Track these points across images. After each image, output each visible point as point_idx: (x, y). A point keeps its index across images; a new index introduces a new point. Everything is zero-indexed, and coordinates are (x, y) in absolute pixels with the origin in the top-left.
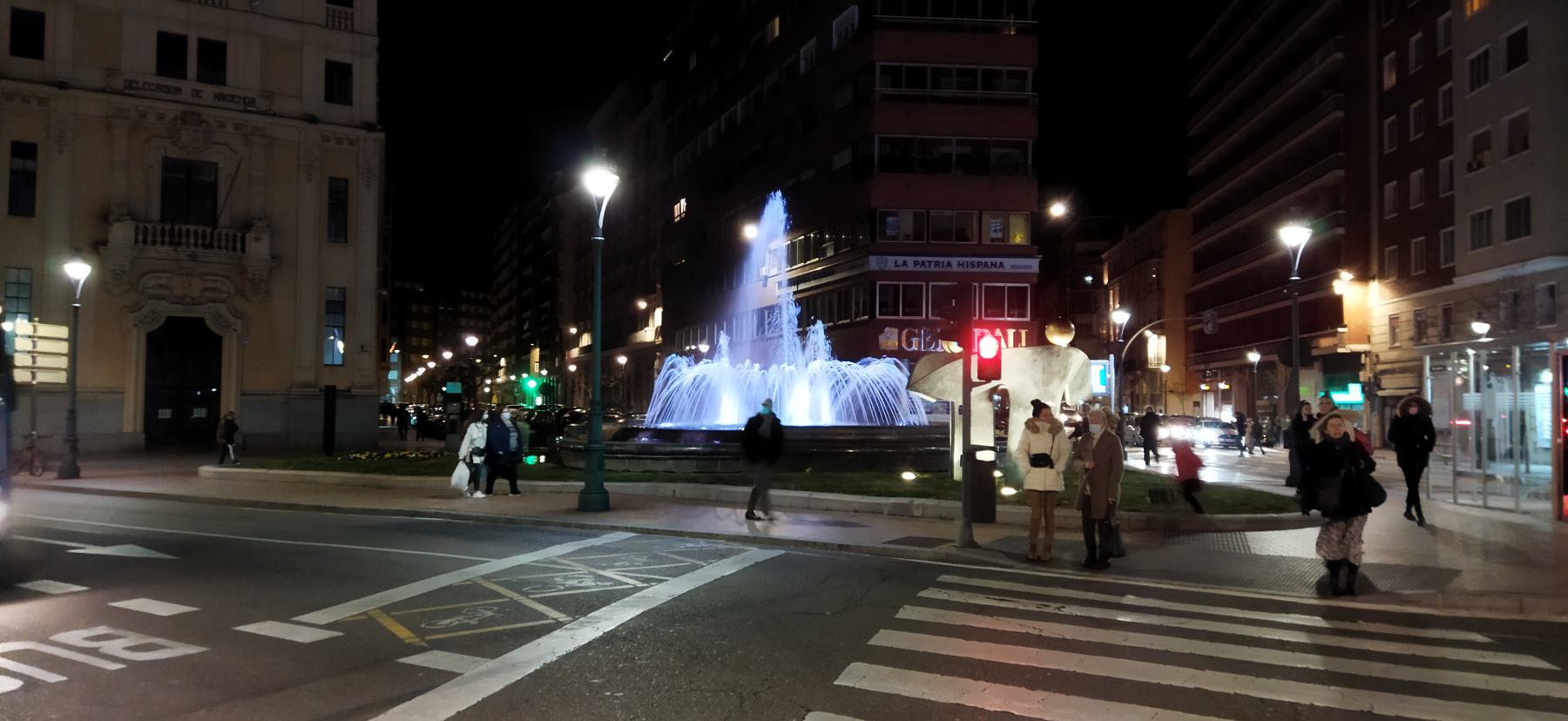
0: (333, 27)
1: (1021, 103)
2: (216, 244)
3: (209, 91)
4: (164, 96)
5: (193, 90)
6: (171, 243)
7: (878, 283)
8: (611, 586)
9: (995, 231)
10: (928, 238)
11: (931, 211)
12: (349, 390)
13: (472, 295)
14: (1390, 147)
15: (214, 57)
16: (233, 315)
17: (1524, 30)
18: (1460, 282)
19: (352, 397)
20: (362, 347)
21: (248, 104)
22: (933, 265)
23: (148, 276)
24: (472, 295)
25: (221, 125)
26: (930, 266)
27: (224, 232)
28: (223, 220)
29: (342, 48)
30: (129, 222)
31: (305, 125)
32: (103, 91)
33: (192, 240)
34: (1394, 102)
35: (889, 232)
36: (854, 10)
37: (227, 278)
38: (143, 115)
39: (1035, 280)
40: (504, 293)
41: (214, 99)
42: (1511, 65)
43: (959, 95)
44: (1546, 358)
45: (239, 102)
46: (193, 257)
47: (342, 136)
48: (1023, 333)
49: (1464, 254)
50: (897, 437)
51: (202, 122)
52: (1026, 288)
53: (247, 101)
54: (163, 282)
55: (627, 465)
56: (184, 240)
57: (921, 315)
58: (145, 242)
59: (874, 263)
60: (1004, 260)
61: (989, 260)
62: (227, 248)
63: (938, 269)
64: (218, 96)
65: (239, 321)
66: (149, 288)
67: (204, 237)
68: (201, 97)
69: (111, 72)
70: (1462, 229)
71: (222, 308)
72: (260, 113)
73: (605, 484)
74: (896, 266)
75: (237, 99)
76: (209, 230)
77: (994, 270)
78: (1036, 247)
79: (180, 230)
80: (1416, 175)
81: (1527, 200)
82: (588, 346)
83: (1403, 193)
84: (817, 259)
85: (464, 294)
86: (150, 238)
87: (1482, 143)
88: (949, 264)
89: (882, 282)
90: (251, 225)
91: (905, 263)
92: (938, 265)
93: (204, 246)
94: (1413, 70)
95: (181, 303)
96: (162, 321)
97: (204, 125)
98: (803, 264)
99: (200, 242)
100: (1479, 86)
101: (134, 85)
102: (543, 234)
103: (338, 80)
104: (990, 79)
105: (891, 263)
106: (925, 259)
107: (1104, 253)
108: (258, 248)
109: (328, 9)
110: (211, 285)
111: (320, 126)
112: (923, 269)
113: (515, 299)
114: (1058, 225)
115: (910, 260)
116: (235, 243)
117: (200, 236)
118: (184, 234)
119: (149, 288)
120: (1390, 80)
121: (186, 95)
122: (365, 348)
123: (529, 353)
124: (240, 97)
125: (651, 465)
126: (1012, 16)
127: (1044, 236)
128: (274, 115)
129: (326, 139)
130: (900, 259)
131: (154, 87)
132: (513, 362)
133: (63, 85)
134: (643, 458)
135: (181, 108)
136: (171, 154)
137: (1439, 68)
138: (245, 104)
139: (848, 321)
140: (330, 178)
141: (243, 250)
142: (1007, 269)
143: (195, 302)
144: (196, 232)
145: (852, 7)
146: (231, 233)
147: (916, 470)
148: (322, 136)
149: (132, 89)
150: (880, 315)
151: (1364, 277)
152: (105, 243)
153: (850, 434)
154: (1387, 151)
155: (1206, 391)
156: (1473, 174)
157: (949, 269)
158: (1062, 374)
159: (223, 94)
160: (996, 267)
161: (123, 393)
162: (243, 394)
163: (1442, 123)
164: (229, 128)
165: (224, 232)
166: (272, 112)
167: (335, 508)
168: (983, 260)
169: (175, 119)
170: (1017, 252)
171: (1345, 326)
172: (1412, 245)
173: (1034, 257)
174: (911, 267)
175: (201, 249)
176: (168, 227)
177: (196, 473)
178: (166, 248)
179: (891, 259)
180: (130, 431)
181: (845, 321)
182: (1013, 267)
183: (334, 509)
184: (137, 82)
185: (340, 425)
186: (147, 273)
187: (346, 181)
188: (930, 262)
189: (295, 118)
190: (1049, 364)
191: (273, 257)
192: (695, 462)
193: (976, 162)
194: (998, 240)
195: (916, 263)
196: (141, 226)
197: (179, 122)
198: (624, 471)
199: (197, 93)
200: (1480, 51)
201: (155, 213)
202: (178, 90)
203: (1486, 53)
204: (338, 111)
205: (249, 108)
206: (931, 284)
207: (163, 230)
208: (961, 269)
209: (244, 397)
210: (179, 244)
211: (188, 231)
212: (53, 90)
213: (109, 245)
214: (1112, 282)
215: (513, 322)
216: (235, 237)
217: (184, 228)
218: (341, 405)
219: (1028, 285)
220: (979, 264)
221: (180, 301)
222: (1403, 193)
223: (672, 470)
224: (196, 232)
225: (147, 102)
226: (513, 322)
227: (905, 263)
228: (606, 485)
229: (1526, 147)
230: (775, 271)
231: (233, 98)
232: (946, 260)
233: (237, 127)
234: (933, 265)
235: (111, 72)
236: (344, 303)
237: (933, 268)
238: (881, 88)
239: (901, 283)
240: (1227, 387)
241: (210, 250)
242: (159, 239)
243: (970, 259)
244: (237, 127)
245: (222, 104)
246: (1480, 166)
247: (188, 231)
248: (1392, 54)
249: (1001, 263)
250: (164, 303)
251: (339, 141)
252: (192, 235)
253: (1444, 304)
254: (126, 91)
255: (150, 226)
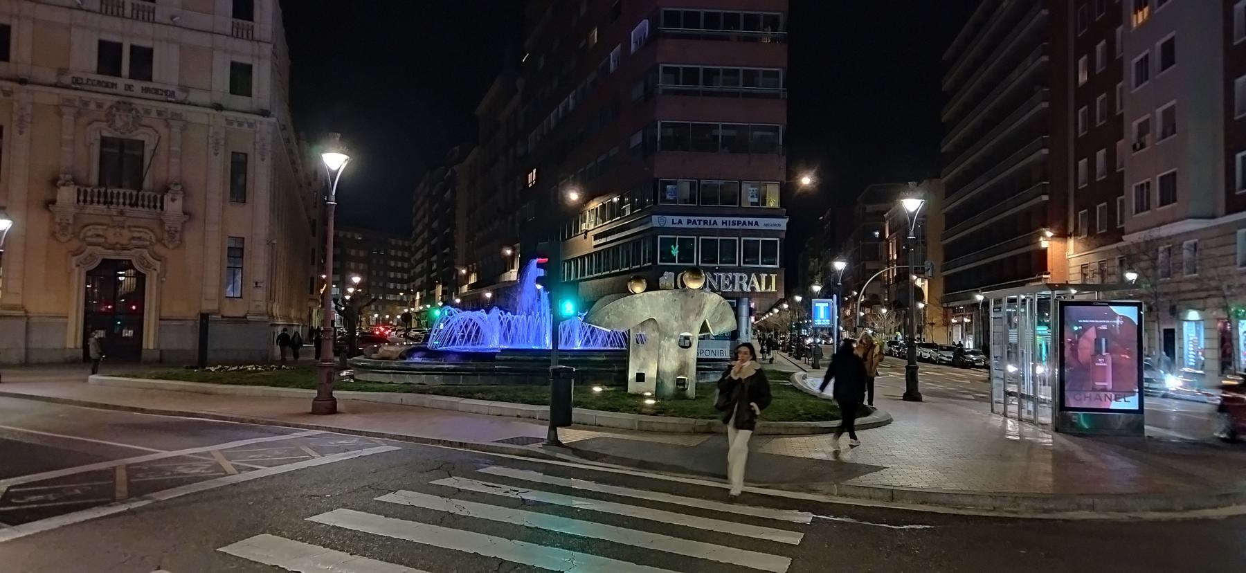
0: (237, 37)
1: (775, 96)
2: (140, 203)
3: (138, 85)
4: (101, 89)
5: (126, 85)
6: (105, 203)
7: (659, 237)
8: (213, 473)
9: (752, 196)
10: (699, 203)
11: (702, 181)
12: (245, 317)
13: (400, 243)
14: (1083, 132)
15: (143, 60)
16: (154, 258)
17: (1173, 39)
18: (1128, 239)
19: (248, 322)
20: (256, 284)
21: (168, 96)
22: (702, 223)
23: (88, 228)
24: (400, 243)
25: (147, 112)
26: (700, 224)
27: (147, 194)
28: (147, 183)
29: (243, 51)
30: (73, 186)
31: (214, 112)
32: (56, 86)
33: (121, 201)
34: (1085, 95)
35: (668, 197)
36: (646, 22)
37: (152, 231)
38: (86, 104)
39: (783, 236)
40: (419, 241)
41: (142, 92)
42: (1165, 66)
43: (724, 90)
44: (1049, 303)
45: (162, 95)
46: (122, 213)
47: (243, 120)
48: (773, 277)
49: (1131, 218)
50: (605, 358)
51: (132, 110)
52: (777, 241)
53: (168, 93)
54: (100, 232)
55: (390, 378)
56: (115, 200)
57: (735, 263)
58: (85, 201)
59: (656, 221)
60: (758, 219)
61: (747, 220)
62: (149, 206)
63: (706, 226)
64: (146, 90)
65: (159, 263)
66: (89, 237)
67: (106, 195)
68: (133, 91)
69: (62, 72)
70: (1130, 197)
71: (146, 253)
72: (177, 103)
73: (334, 392)
74: (673, 223)
75: (160, 92)
76: (134, 193)
77: (750, 227)
78: (785, 210)
79: (112, 193)
80: (1101, 154)
81: (1174, 174)
82: (475, 283)
83: (1092, 166)
84: (619, 218)
85: (393, 242)
86: (89, 199)
87: (1144, 128)
88: (715, 222)
89: (703, 237)
90: (169, 189)
91: (680, 222)
92: (707, 223)
93: (131, 205)
94: (1099, 69)
95: (113, 249)
96: (98, 262)
97: (134, 112)
98: (610, 221)
99: (128, 202)
100: (1142, 83)
101: (80, 81)
102: (446, 196)
103: (241, 77)
104: (750, 78)
105: (669, 221)
106: (697, 218)
107: (885, 213)
108: (174, 207)
109: (233, 22)
110: (136, 235)
111: (225, 113)
112: (694, 226)
113: (426, 246)
114: (806, 194)
115: (684, 219)
116: (155, 202)
117: (146, 199)
118: (115, 195)
119: (89, 237)
120: (1083, 78)
121: (120, 89)
122: (259, 285)
123: (435, 288)
124: (162, 91)
125: (409, 379)
126: (770, 29)
127: (791, 200)
128: (190, 104)
129: (230, 122)
130: (676, 219)
131: (95, 83)
132: (425, 295)
133: (23, 82)
134: (403, 373)
135: (117, 99)
136: (106, 134)
137: (1115, 68)
138: (166, 95)
139: (639, 266)
140: (233, 153)
141: (162, 208)
142: (761, 227)
143: (124, 248)
144: (125, 194)
145: (644, 20)
146: (153, 194)
147: (600, 386)
148: (226, 120)
149: (79, 84)
150: (660, 262)
151: (1063, 235)
152: (54, 202)
153: (567, 356)
154: (1081, 135)
155: (956, 324)
156: (1137, 153)
157: (715, 226)
158: (697, 311)
159: (148, 88)
160: (752, 225)
161: (67, 317)
162: (161, 319)
163: (1118, 113)
164: (154, 114)
165: (147, 194)
166: (187, 102)
167: (142, 409)
168: (742, 219)
169: (111, 107)
170: (772, 213)
171: (1049, 274)
172: (1098, 208)
173: (782, 217)
174: (685, 225)
175: (128, 207)
176: (102, 190)
177: (86, 381)
178: (102, 207)
179: (669, 218)
180: (73, 347)
181: (637, 266)
182: (766, 225)
183: (142, 410)
184: (82, 79)
185: (212, 345)
186: (87, 225)
187: (246, 155)
188: (700, 221)
189: (204, 106)
190: (686, 302)
191: (185, 213)
192: (442, 376)
193: (738, 144)
194: (757, 204)
195: (689, 221)
196: (82, 189)
197: (114, 109)
198: (390, 383)
199: (129, 87)
200: (1142, 56)
201: (94, 179)
202: (114, 85)
203: (1147, 56)
204: (241, 101)
205: (169, 99)
206: (701, 238)
207: (99, 192)
208: (724, 227)
209: (163, 322)
210: (112, 203)
211: (118, 193)
212: (15, 86)
213: (57, 203)
214: (892, 235)
215: (425, 264)
216: (155, 198)
217: (115, 191)
218: (212, 329)
219: (778, 239)
220: (739, 223)
221: (112, 247)
222: (1092, 166)
223: (425, 382)
224: (125, 194)
225: (89, 95)
226: (425, 264)
227: (680, 222)
228: (336, 394)
229: (1174, 132)
230: (592, 227)
231: (156, 91)
232: (713, 219)
233: (160, 113)
234: (702, 223)
235: (62, 72)
236: (242, 249)
237: (702, 226)
238: (663, 84)
239: (719, 238)
240: (969, 321)
241: (135, 208)
242: (96, 199)
243: (732, 219)
244: (160, 113)
245: (148, 95)
246: (1142, 146)
247: (118, 193)
248: (1085, 57)
249: (756, 222)
250: (100, 248)
251: (240, 124)
252: (121, 196)
253: (1120, 256)
254: (74, 86)
255: (89, 190)
